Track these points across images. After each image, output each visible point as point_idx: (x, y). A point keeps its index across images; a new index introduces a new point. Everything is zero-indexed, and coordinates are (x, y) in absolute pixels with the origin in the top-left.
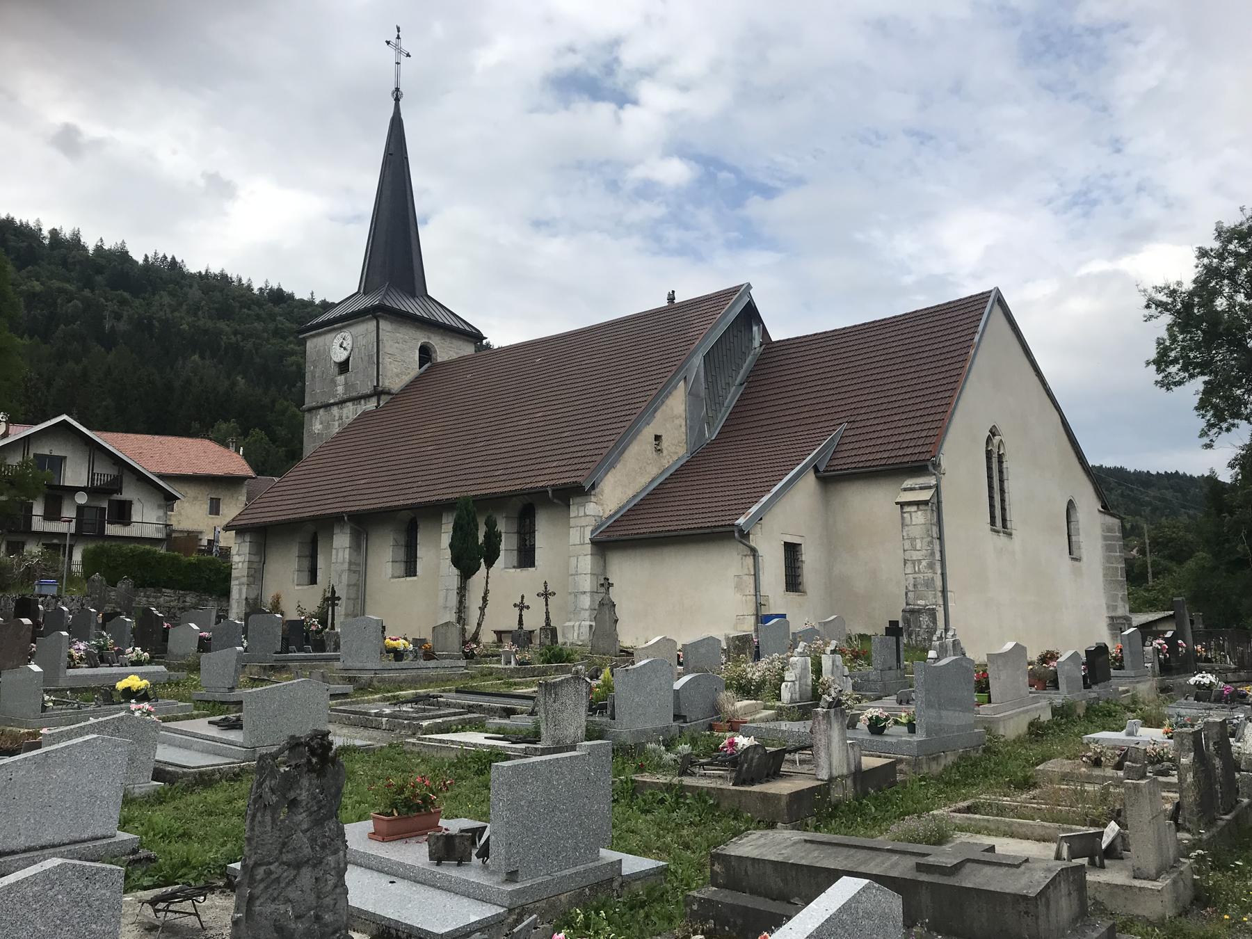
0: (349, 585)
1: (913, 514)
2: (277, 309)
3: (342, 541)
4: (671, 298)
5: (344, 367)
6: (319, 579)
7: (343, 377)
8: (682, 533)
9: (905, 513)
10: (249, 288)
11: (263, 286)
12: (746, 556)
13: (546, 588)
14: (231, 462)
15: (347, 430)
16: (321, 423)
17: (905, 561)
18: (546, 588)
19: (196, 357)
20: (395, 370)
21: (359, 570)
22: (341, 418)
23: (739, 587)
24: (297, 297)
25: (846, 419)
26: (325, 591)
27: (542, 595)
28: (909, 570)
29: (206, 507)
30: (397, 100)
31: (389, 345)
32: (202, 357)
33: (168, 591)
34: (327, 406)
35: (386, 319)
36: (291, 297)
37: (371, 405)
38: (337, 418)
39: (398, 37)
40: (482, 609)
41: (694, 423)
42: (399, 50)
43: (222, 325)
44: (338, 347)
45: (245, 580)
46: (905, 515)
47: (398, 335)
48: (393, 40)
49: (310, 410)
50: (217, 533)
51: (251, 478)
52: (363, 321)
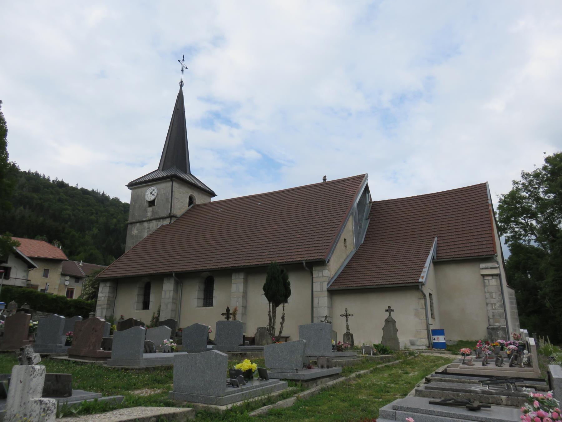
0: (172, 310)
1: (490, 281)
2: (60, 190)
3: (168, 287)
4: (325, 179)
5: (152, 203)
6: (151, 305)
7: (151, 208)
8: (386, 286)
9: (485, 280)
10: (48, 180)
11: (55, 179)
12: (420, 299)
13: (346, 312)
14: (56, 252)
15: (154, 235)
16: (137, 230)
17: (487, 304)
18: (346, 312)
19: (22, 208)
20: (178, 206)
21: (177, 302)
22: (149, 228)
23: (417, 315)
24: (70, 185)
25: (436, 235)
26: (154, 313)
27: (344, 315)
28: (489, 308)
29: (42, 273)
30: (181, 86)
31: (176, 194)
32: (25, 208)
33: (40, 312)
34: (141, 222)
35: (176, 181)
36: (67, 185)
37: (167, 222)
38: (146, 228)
39: (183, 60)
40: (282, 324)
41: (357, 234)
42: (183, 65)
43: (35, 195)
44: (149, 194)
45: (105, 306)
46: (486, 281)
47: (180, 190)
48: (181, 60)
49: (131, 223)
50: (47, 286)
51: (66, 260)
52: (164, 182)
